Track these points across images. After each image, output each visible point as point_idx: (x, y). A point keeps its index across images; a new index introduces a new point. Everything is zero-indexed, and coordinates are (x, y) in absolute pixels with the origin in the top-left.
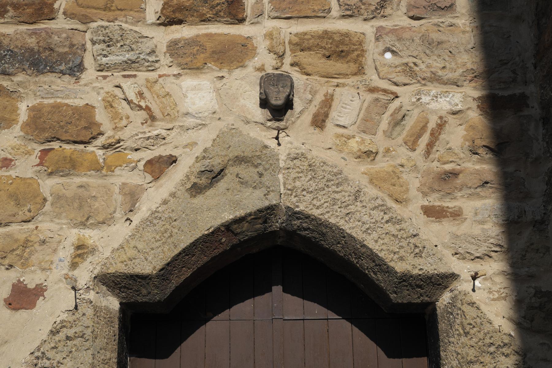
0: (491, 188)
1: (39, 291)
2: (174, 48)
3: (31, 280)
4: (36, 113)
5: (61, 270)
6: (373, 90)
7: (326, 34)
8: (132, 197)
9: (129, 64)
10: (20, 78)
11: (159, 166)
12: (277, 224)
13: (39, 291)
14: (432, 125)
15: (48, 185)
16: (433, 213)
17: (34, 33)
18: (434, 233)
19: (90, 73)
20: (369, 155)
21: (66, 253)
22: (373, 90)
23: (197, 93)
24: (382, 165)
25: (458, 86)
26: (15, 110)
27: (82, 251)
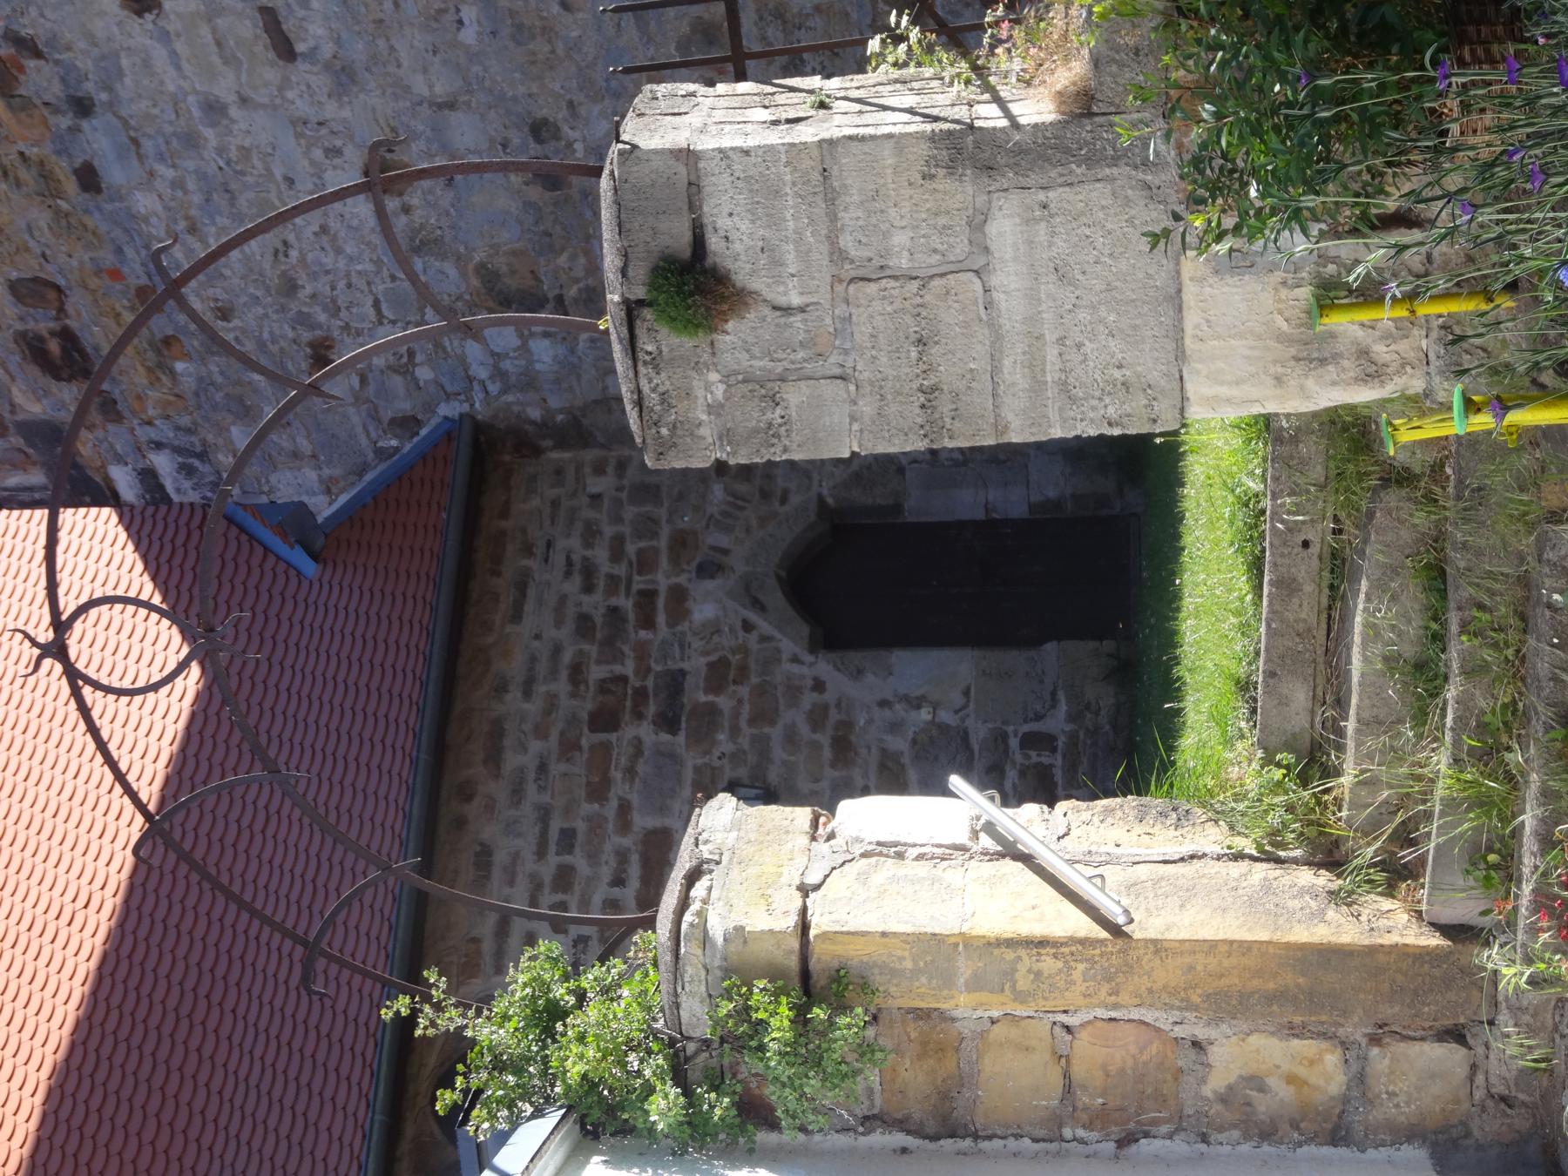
0: (1011, 216)
1: (816, 679)
2: (671, 624)
3: (810, 683)
4: (707, 691)
5: (805, 670)
6: (707, 526)
7: (671, 548)
8: (764, 639)
9: (682, 646)
10: (685, 700)
11: (747, 627)
12: (783, 574)
13: (816, 679)
14: (731, 499)
15: (755, 680)
16: (784, 500)
17: (655, 695)
18: (796, 499)
19: (686, 666)
20: (748, 531)
21: (795, 669)
22: (707, 526)
23: (703, 611)
24: (754, 523)
25: (1180, 291)
26: (706, 703)
27: (795, 659)
